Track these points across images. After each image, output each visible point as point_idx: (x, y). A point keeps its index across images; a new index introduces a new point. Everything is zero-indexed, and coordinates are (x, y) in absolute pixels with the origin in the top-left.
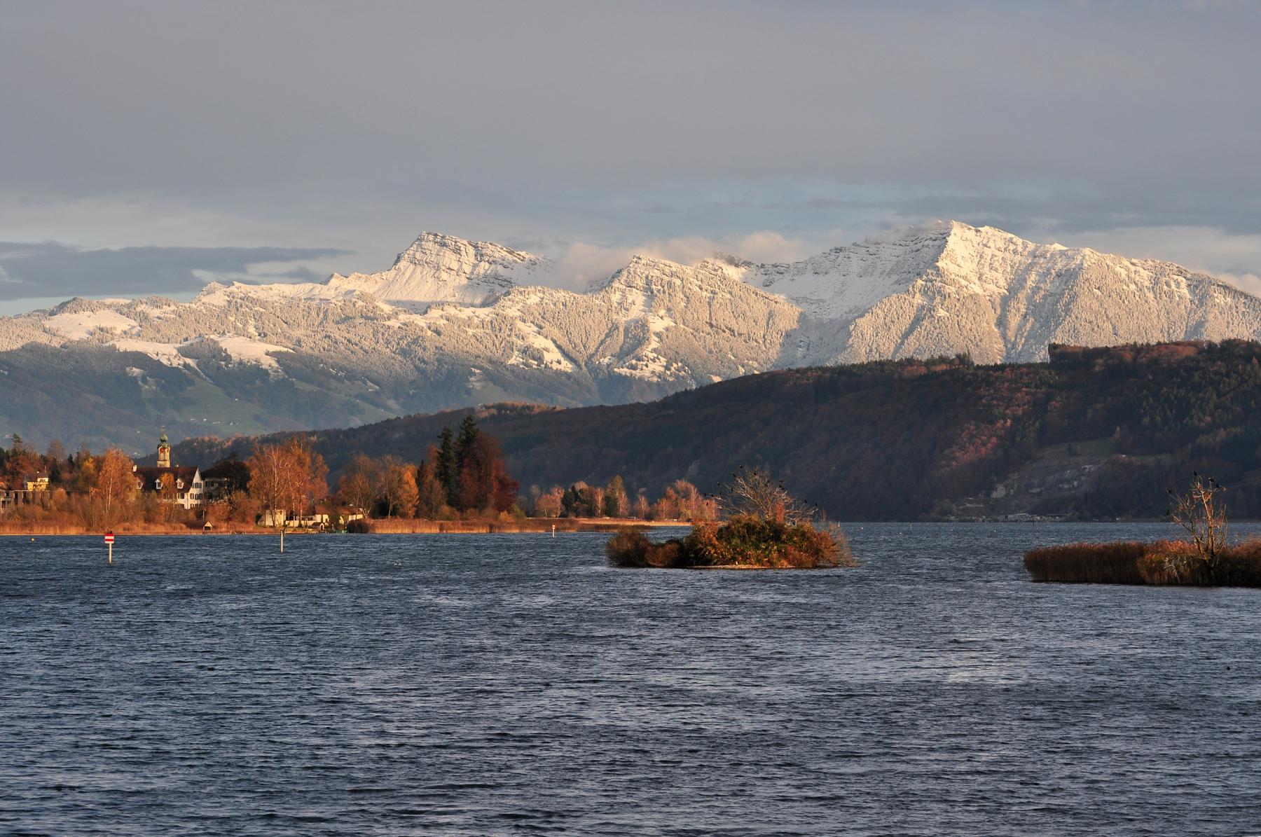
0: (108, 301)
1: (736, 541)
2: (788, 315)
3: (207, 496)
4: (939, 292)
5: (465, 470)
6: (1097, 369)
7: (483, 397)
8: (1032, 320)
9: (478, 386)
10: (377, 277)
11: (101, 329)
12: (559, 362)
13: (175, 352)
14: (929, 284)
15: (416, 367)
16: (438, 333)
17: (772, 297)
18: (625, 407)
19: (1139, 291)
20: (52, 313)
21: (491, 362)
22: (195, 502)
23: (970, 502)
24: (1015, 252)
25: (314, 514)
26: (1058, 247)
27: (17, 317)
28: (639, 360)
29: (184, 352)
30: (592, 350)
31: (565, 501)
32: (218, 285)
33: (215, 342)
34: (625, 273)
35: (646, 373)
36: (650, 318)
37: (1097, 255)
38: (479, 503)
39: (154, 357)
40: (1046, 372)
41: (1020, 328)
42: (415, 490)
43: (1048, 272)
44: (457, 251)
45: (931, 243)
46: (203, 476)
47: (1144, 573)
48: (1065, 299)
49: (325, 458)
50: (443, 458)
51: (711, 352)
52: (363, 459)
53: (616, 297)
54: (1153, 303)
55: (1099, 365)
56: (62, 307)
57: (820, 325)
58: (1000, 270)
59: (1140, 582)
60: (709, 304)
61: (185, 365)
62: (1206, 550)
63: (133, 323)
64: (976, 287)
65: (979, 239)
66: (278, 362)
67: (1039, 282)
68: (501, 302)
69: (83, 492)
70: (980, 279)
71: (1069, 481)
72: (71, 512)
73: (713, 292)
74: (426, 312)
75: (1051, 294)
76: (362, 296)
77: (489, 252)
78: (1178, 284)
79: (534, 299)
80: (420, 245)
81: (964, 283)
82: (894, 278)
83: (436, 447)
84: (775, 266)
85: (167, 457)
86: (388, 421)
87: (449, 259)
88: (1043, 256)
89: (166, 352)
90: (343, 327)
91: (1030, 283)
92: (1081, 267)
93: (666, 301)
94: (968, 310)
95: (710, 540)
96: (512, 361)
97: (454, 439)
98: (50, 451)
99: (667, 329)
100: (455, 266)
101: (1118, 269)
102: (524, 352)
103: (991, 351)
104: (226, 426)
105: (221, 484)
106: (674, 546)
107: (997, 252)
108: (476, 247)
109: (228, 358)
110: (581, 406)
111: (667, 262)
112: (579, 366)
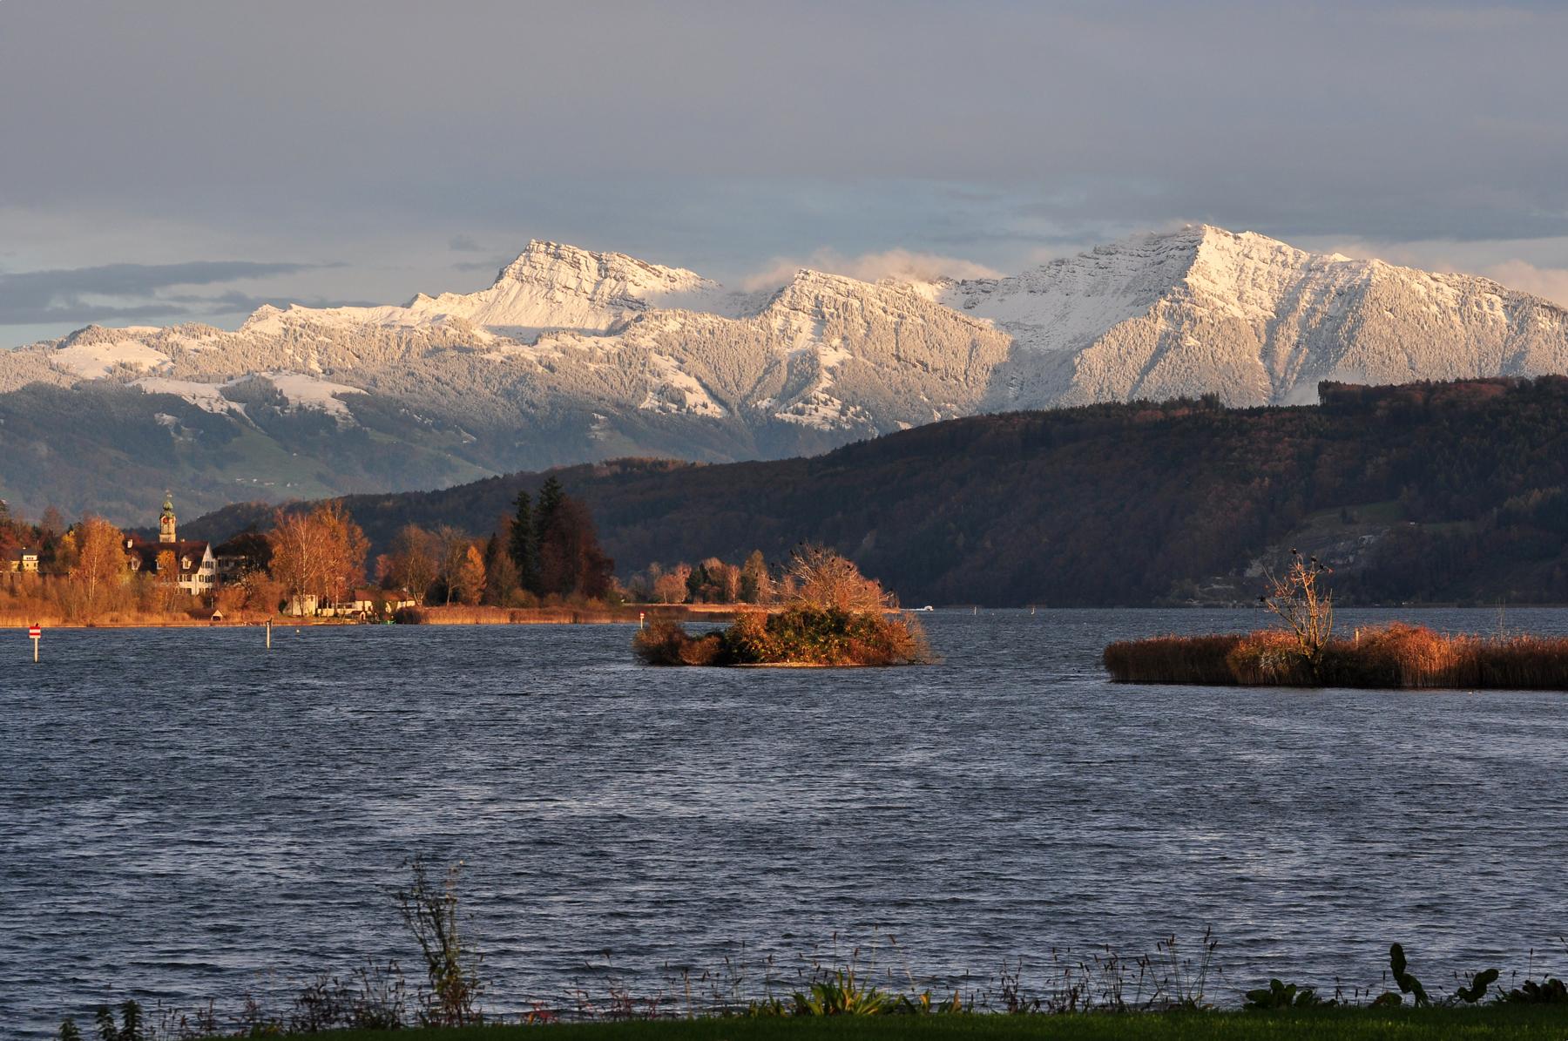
0: (132, 329)
1: (790, 633)
2: (996, 343)
3: (221, 579)
4: (1188, 315)
5: (547, 545)
6: (1379, 413)
7: (607, 447)
8: (1306, 350)
9: (601, 436)
10: (473, 297)
11: (123, 366)
12: (705, 406)
13: (216, 394)
14: (1175, 305)
15: (522, 412)
16: (551, 368)
17: (975, 322)
18: (782, 462)
19: (1440, 312)
20: (61, 346)
21: (618, 405)
22: (205, 586)
23: (1217, 583)
24: (1284, 264)
25: (353, 600)
26: (1339, 257)
27: (16, 349)
28: (807, 402)
29: (229, 394)
30: (746, 390)
31: (691, 584)
32: (271, 309)
33: (269, 382)
34: (789, 292)
35: (816, 419)
36: (821, 348)
37: (1388, 269)
38: (564, 587)
39: (191, 401)
40: (1315, 418)
41: (1290, 361)
42: (481, 570)
43: (1327, 289)
44: (575, 264)
45: (1177, 253)
46: (215, 554)
47: (1234, 668)
48: (1349, 324)
49: (364, 529)
50: (519, 530)
51: (898, 392)
52: (413, 531)
53: (777, 323)
54: (1460, 329)
55: (1382, 408)
56: (73, 337)
57: (1037, 358)
58: (1266, 288)
59: (1232, 682)
60: (896, 331)
61: (231, 412)
62: (1307, 643)
63: (164, 357)
64: (1238, 304)
65: (1238, 249)
66: (348, 406)
67: (1315, 302)
68: (631, 330)
69: (59, 574)
70: (1240, 298)
71: (1343, 556)
72: (45, 598)
73: (901, 317)
74: (536, 343)
75: (1331, 318)
76: (454, 323)
77: (616, 266)
78: (1492, 305)
79: (673, 326)
80: (528, 257)
81: (1220, 304)
82: (1132, 297)
83: (511, 516)
84: (980, 282)
85: (172, 530)
86: (484, 481)
87: (565, 274)
88: (1320, 269)
89: (206, 396)
90: (430, 361)
91: (1304, 304)
92: (1368, 283)
93: (841, 328)
94: (1225, 338)
95: (758, 632)
96: (645, 405)
97: (533, 506)
98: (44, 521)
99: (842, 363)
100: (573, 283)
101: (1415, 286)
102: (661, 393)
103: (1252, 389)
104: (269, 483)
105: (238, 564)
106: (714, 639)
107: (1261, 265)
108: (599, 259)
109: (284, 402)
110: (733, 461)
111: (843, 279)
112: (730, 411)
